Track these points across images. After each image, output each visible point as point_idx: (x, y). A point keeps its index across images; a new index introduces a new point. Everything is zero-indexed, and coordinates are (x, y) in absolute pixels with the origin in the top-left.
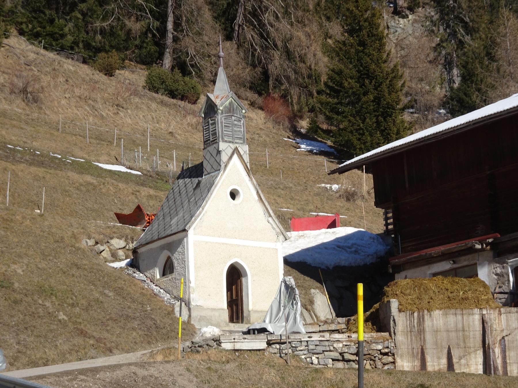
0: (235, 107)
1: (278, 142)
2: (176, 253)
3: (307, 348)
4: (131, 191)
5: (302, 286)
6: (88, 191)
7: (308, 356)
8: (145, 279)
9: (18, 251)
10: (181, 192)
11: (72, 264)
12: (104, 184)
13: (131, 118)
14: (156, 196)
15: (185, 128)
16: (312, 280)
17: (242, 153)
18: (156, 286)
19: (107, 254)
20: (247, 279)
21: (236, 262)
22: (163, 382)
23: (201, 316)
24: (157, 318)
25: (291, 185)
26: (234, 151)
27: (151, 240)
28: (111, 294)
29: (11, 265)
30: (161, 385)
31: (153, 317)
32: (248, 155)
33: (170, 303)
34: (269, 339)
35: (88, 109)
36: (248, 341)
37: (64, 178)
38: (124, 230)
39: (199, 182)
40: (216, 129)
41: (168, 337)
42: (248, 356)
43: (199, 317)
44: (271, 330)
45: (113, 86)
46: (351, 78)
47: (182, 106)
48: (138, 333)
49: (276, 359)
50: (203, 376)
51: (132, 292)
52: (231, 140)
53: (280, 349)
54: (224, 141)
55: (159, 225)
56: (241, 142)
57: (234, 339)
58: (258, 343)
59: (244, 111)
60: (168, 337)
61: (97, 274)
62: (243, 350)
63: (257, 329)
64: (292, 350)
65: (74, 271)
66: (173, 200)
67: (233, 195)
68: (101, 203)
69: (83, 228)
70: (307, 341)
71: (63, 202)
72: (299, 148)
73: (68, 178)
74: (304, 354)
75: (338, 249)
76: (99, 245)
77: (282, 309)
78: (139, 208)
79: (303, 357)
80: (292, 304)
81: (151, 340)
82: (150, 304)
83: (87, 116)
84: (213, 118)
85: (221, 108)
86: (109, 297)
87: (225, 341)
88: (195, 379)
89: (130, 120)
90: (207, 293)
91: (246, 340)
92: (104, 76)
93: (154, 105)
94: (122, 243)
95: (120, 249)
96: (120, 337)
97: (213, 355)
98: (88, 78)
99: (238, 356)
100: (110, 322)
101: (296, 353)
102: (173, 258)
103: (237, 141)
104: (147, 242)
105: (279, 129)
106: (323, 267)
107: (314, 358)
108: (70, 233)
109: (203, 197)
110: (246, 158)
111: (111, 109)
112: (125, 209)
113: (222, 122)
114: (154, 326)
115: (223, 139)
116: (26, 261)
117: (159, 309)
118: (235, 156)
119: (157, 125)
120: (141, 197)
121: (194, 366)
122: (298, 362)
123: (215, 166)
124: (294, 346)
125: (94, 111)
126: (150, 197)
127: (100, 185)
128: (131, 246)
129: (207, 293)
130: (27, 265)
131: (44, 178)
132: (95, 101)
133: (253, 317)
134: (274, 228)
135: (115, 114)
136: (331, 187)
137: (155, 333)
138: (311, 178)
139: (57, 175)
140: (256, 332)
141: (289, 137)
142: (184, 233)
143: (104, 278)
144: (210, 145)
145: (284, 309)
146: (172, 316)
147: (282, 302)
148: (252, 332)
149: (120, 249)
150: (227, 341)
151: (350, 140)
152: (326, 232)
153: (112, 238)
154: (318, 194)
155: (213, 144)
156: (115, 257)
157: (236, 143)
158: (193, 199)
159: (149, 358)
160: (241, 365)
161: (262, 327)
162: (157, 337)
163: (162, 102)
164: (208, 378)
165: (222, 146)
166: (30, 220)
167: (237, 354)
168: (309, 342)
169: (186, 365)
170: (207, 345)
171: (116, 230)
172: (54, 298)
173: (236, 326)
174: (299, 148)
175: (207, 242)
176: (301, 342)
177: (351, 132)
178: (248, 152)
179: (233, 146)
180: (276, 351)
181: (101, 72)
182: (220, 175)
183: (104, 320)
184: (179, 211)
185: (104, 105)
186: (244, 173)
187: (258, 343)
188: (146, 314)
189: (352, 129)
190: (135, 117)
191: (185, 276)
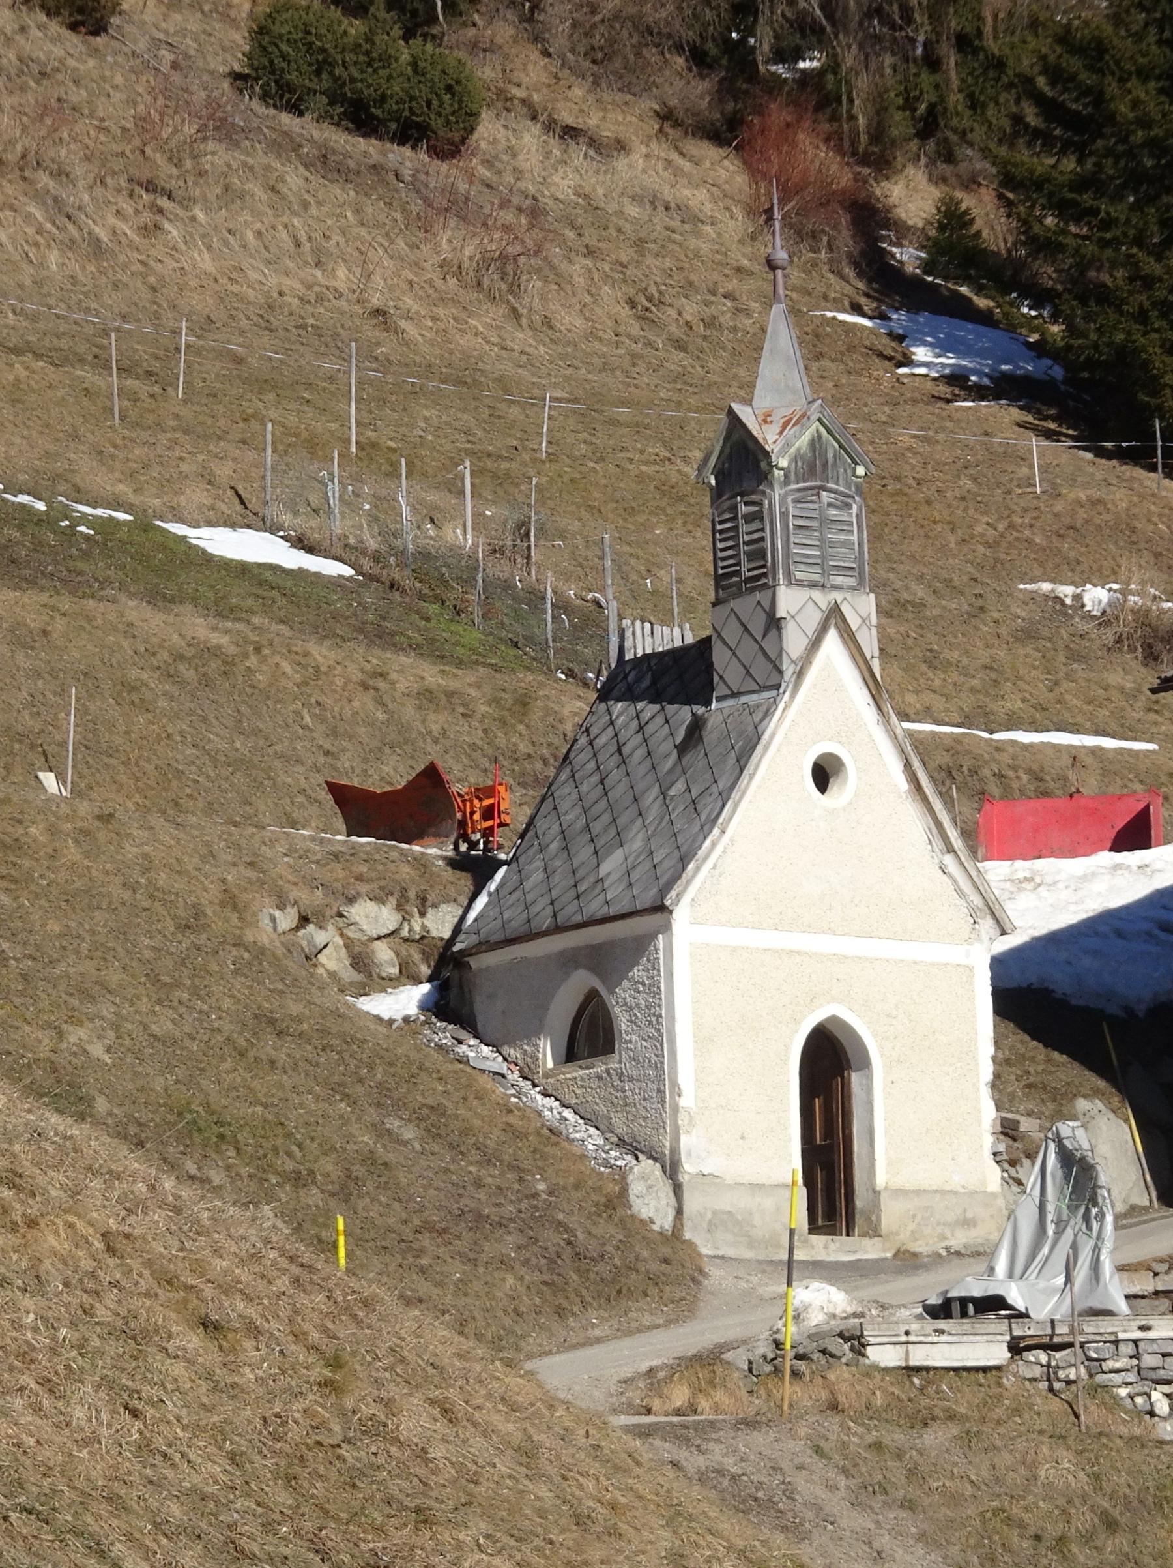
0: (830, 455)
1: (817, 336)
2: (625, 983)
3: (1135, 1362)
4: (357, 676)
5: (1044, 1088)
6: (206, 681)
7: (1138, 1388)
8: (504, 1068)
9: (72, 970)
10: (626, 750)
11: (256, 1016)
12: (258, 650)
13: (209, 248)
14: (450, 695)
15: (430, 282)
16: (1076, 1065)
17: (854, 622)
18: (546, 1094)
19: (339, 960)
20: (870, 1078)
21: (834, 1019)
22: (757, 1490)
23: (715, 1213)
24: (573, 1222)
25: (920, 592)
26: (827, 619)
27: (523, 930)
28: (408, 1134)
29: (65, 1027)
30: (756, 1500)
31: (561, 1216)
32: (874, 631)
33: (607, 1164)
34: (1016, 1333)
35: (39, 214)
36: (950, 1338)
37: (115, 629)
38: (390, 865)
39: (696, 727)
40: (762, 539)
41: (619, 1292)
42: (950, 1388)
43: (709, 1215)
44: (1020, 1305)
45: (116, 87)
46: (1144, 75)
47: (407, 173)
48: (522, 1279)
49: (1039, 1400)
50: (864, 1469)
51: (477, 1123)
52: (817, 578)
53: (1049, 1366)
54: (792, 582)
55: (548, 873)
56: (852, 582)
57: (907, 1333)
58: (984, 1347)
59: (860, 471)
60: (619, 1292)
61: (346, 1056)
62: (936, 1368)
63: (974, 1300)
64: (1088, 1369)
65: (268, 1046)
66: (596, 778)
67: (824, 774)
68: (256, 732)
69: (251, 864)
70: (1135, 1342)
71: (127, 733)
72: (907, 361)
73: (129, 629)
74: (1127, 1384)
75: (1163, 936)
76: (311, 927)
77: (1051, 1230)
78: (431, 776)
79: (1123, 1392)
80: (1086, 1218)
81: (565, 1304)
82: (541, 1170)
83: (36, 245)
84: (753, 497)
85: (784, 463)
86: (405, 1143)
87: (879, 1340)
88: (842, 1481)
89: (206, 256)
90: (733, 1132)
91: (944, 1338)
92: (67, 33)
93: (294, 179)
94: (384, 917)
95: (379, 938)
96: (465, 1295)
97: (844, 1387)
98: (12, 56)
99: (922, 1389)
100: (426, 1240)
101: (1100, 1378)
102: (611, 1001)
103: (839, 580)
104: (509, 934)
105: (815, 265)
106: (1113, 1009)
107: (1156, 1396)
108: (214, 890)
109: (721, 785)
110: (869, 642)
111: (128, 207)
112: (344, 750)
113: (785, 515)
114: (569, 1250)
115: (788, 574)
116: (106, 1010)
117: (577, 1187)
118: (832, 642)
119: (318, 273)
120: (394, 700)
121: (833, 1437)
122: (1110, 1410)
123: (760, 670)
124: (1095, 1356)
125: (62, 220)
126: (427, 696)
127: (246, 656)
128: (417, 928)
129: (733, 1132)
130: (116, 1027)
131: (45, 633)
132: (61, 174)
133: (891, 1214)
134: (961, 893)
135: (144, 230)
136: (1077, 598)
137: (575, 1277)
138: (979, 529)
139: (89, 619)
140: (971, 1309)
141: (857, 309)
142: (657, 918)
143: (371, 1068)
144: (739, 594)
145: (1059, 1233)
146: (620, 1212)
147: (1050, 1208)
148: (956, 1308)
149: (379, 938)
150: (885, 1340)
151: (1137, 351)
152: (1117, 867)
153: (351, 900)
154: (1028, 634)
155: (753, 589)
156: (370, 979)
157: (835, 587)
158: (680, 786)
159: (647, 1396)
160: (968, 1433)
161: (990, 1293)
162: (584, 1292)
163: (325, 163)
164: (880, 1477)
165: (788, 600)
166: (76, 841)
167: (916, 1381)
168: (1141, 1345)
169: (808, 1437)
170: (824, 1352)
171: (364, 869)
172: (232, 1153)
173: (832, 1246)
174: (907, 361)
175: (734, 950)
176: (1116, 1342)
177: (1142, 317)
178: (874, 619)
179: (823, 599)
180: (1037, 1372)
181: (58, 14)
182: (781, 706)
183: (408, 1234)
184: (626, 827)
185: (99, 191)
186: (860, 696)
187: (984, 1347)
188: (535, 1207)
189: (1147, 304)
190: (226, 243)
191: (659, 1068)
